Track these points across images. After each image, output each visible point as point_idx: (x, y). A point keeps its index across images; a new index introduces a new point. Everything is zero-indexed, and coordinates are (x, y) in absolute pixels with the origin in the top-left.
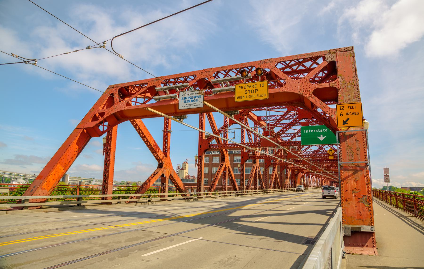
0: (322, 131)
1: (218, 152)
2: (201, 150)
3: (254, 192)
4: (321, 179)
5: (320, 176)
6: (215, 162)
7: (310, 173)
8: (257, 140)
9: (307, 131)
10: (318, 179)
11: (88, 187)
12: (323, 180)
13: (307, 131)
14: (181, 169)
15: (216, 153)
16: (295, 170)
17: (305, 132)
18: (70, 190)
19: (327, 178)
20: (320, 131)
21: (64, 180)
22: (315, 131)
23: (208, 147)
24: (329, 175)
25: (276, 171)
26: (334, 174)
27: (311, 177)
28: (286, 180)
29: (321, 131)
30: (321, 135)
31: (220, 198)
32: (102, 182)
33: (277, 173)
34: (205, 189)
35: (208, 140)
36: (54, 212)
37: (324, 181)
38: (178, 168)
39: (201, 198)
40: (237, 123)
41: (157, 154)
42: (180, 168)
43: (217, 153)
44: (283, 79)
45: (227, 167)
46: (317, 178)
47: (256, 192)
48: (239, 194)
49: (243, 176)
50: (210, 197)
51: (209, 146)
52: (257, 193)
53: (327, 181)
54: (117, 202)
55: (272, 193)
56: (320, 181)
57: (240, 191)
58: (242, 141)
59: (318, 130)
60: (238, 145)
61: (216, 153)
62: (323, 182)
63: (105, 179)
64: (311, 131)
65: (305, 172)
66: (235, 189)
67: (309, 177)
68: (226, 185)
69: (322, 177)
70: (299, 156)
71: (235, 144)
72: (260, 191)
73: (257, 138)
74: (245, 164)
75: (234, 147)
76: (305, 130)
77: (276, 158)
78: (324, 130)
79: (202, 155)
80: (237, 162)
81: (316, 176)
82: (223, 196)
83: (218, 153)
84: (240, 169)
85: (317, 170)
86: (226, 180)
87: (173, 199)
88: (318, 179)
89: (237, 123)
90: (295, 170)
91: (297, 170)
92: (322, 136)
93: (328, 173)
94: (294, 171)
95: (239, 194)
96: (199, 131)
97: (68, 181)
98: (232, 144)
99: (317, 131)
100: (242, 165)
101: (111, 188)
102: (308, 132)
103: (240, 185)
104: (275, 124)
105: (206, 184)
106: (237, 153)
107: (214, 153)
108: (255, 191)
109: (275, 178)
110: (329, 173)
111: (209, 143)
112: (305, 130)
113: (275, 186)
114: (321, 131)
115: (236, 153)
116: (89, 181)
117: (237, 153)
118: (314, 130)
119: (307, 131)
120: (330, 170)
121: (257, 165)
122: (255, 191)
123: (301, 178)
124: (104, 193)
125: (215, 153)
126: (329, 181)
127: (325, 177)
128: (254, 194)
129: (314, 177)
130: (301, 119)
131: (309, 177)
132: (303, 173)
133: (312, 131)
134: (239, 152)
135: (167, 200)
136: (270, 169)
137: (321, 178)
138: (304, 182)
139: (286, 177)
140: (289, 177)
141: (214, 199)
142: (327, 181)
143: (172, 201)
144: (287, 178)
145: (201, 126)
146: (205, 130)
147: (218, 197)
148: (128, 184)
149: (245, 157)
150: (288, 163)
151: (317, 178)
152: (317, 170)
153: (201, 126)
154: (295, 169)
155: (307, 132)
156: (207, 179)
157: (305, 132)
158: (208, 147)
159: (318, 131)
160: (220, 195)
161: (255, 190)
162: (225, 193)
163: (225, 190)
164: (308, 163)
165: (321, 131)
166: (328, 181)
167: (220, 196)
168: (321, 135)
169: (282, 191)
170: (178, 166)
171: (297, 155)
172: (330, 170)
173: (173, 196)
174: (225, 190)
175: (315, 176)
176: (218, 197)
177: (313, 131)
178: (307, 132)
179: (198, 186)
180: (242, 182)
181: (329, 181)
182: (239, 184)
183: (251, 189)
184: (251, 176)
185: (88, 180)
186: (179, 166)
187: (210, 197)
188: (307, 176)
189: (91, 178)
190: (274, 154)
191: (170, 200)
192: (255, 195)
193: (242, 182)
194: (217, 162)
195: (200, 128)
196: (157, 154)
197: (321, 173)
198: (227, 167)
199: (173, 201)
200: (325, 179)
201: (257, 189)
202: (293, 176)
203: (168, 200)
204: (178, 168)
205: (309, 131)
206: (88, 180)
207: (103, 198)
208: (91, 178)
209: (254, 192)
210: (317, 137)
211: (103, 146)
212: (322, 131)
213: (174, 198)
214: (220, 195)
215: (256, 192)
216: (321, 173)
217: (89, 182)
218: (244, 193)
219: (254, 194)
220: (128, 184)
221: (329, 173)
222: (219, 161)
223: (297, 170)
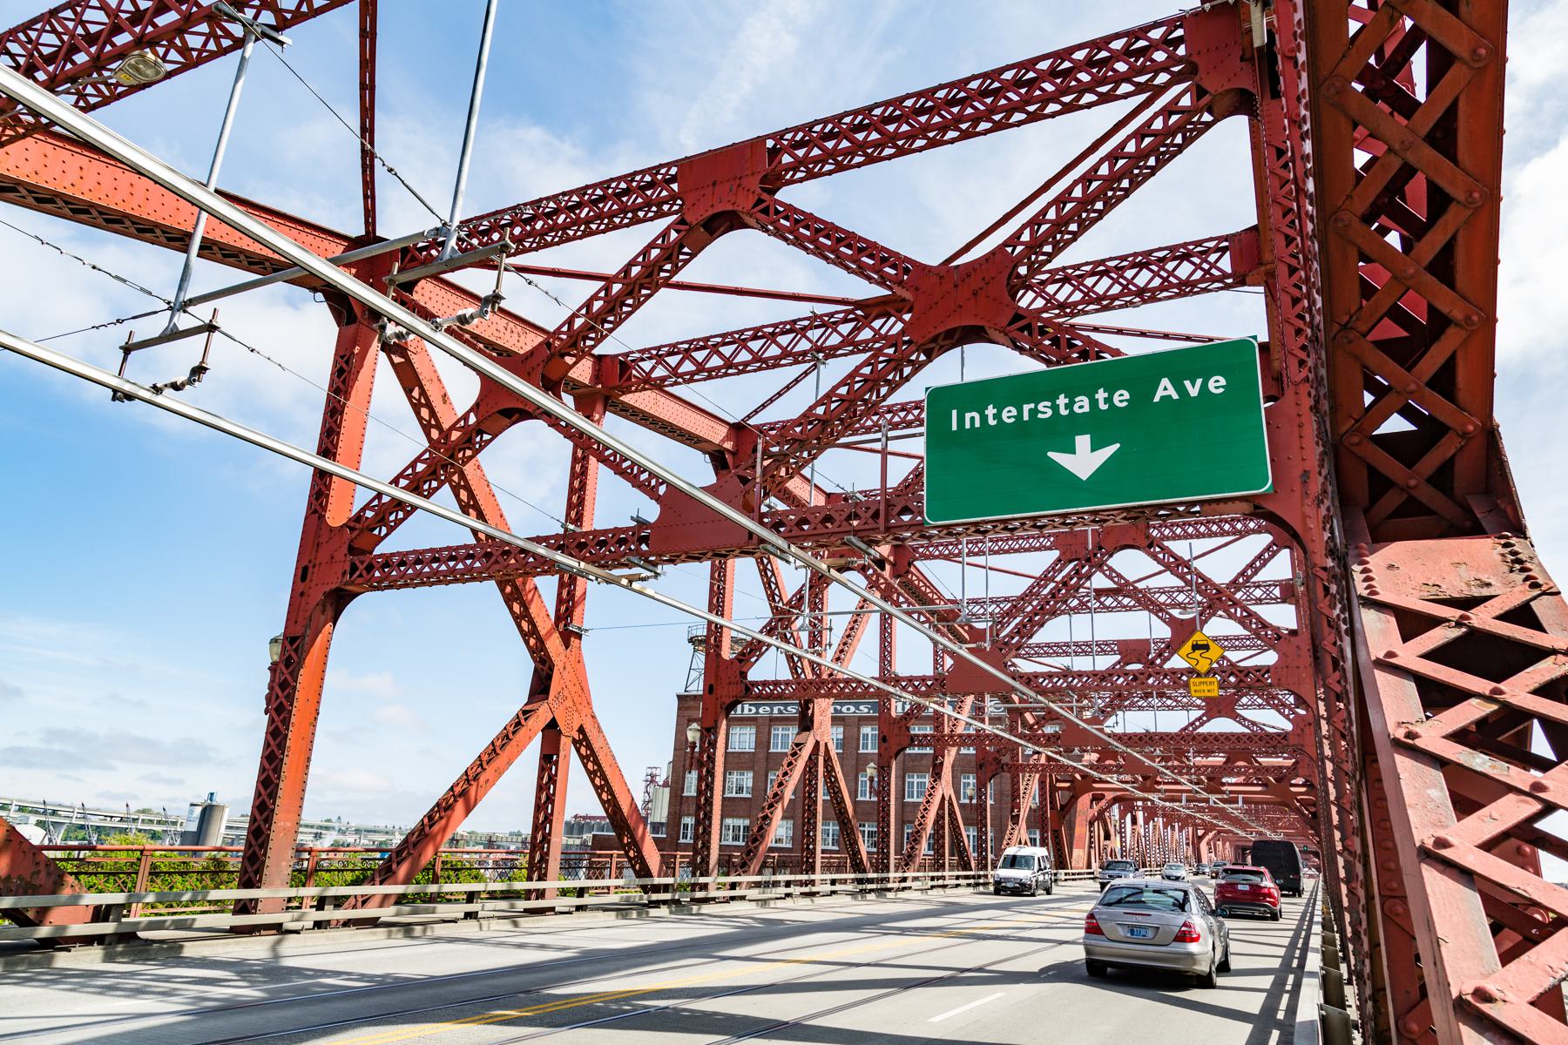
0: (1086, 409)
1: (750, 705)
2: (302, 594)
3: (933, 879)
4: (1195, 832)
5: (1185, 821)
6: (737, 750)
7: (1140, 803)
8: (943, 666)
9: (972, 419)
10: (1180, 830)
11: (200, 856)
12: (1200, 838)
13: (972, 419)
14: (661, 783)
15: (743, 710)
16: (1059, 785)
17: (954, 428)
18: (99, 870)
19: (1219, 832)
20: (1072, 411)
21: (204, 826)
22: (1034, 412)
23: (344, 574)
24: (1223, 814)
25: (943, 781)
26: (1247, 812)
27: (1146, 822)
28: (1010, 828)
29: (1082, 404)
30: (1078, 439)
31: (789, 903)
33: (950, 792)
34: (681, 863)
35: (740, 661)
37: (1208, 844)
38: (652, 781)
39: (706, 901)
42: (657, 779)
43: (746, 711)
45: (947, 798)
46: (1173, 828)
47: (941, 882)
48: (870, 886)
49: (888, 815)
50: (743, 898)
51: (348, 569)
52: (944, 886)
53: (1220, 843)
54: (462, 915)
55: (918, 895)
56: (1188, 844)
57: (875, 875)
58: (882, 669)
59: (1053, 398)
60: (870, 686)
61: (743, 710)
62: (1203, 846)
64: (1005, 415)
65: (1109, 796)
66: (858, 866)
67: (1134, 821)
68: (814, 849)
69: (1196, 826)
70: (1014, 679)
71: (860, 682)
72: (958, 878)
73: (942, 657)
74: (894, 766)
75: (851, 690)
76: (954, 412)
77: (1021, 745)
78: (1101, 395)
79: (716, 722)
81: (1170, 818)
82: (802, 894)
83: (750, 710)
84: (974, 801)
85: (1160, 787)
86: (815, 828)
87: (579, 908)
88: (1180, 831)
90: (1059, 785)
91: (1067, 785)
92: (1083, 442)
93: (1215, 803)
94: (1054, 789)
95: (870, 886)
96: (710, 623)
97: (223, 830)
98: (847, 682)
99: (1050, 412)
100: (883, 768)
101: (279, 861)
102: (977, 424)
103: (875, 850)
104: (1036, 614)
105: (830, 847)
108: (939, 878)
109: (940, 817)
110: (1221, 805)
111: (744, 675)
112: (954, 412)
113: (986, 858)
114: (1082, 404)
116: (315, 831)
118: (1026, 408)
119: (968, 416)
120: (1224, 788)
121: (817, 743)
122: (939, 878)
123: (1091, 824)
124: (247, 883)
126: (1228, 843)
127: (1208, 828)
128: (932, 887)
129: (1160, 821)
130: (1219, 712)
131: (1134, 821)
132: (1103, 803)
133: (1008, 415)
134: (779, 710)
135: (552, 909)
137: (1190, 829)
138: (1107, 842)
139: (1012, 817)
140: (1024, 814)
141: (389, 937)
142: (1220, 843)
143: (576, 914)
144: (1015, 819)
145: (717, 601)
146: (730, 619)
147: (781, 898)
148: (457, 841)
149: (895, 736)
150: (988, 736)
151: (1173, 828)
152: (1160, 787)
153: (717, 601)
154: (1057, 781)
155: (968, 426)
156: (747, 822)
157: (954, 428)
158: (344, 574)
159: (1055, 408)
160: (788, 890)
161: (935, 874)
162: (812, 882)
163: (811, 869)
164: (1085, 729)
165: (1076, 409)
166: (1224, 844)
167: (788, 895)
168: (1078, 439)
169: (981, 881)
170: (649, 771)
171: (1096, 729)
172: (1224, 788)
173: (581, 892)
174: (811, 869)
175: (1163, 817)
176: (781, 898)
177: (1014, 412)
178: (968, 426)
179: (696, 852)
180: (881, 840)
181: (1228, 843)
182: (833, 845)
183: (922, 867)
184: (776, 795)
185: (312, 827)
186: (654, 771)
187: (743, 898)
188: (1122, 816)
189: (326, 821)
190: (1003, 727)
191: (566, 909)
192: (934, 892)
193: (881, 840)
194: (747, 750)
195: (710, 611)
197: (1184, 803)
198: (947, 798)
199: (581, 914)
200: (1211, 835)
201: (814, 872)
202: (1046, 812)
203: (557, 909)
204: (652, 781)
205: (984, 418)
206: (312, 827)
207: (244, 907)
208: (329, 821)
209: (933, 879)
211: (269, 672)
212: (1086, 409)
213: (587, 900)
214: (788, 890)
215: (941, 882)
216: (1184, 803)
217: (316, 834)
218: (889, 885)
219: (932, 887)
220: (457, 841)
221: (1221, 805)
222: (753, 745)
223: (1067, 785)
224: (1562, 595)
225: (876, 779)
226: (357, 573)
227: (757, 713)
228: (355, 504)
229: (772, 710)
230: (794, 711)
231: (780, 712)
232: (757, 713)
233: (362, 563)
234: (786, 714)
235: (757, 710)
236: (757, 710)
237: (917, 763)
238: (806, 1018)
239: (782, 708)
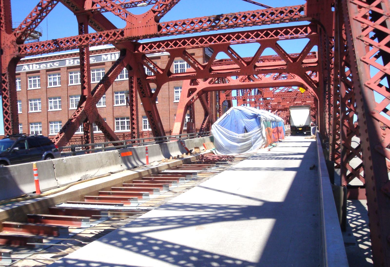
15: (33, 68)
32: (18, 99)
36: (48, 126)
40: (38, 69)
41: (25, 39)
44: (96, 243)
61: (33, 68)
63: (80, 29)
76: (229, 51)
80: (121, 79)
83: (36, 67)
89: (38, 69)
106: (74, 64)
107: (29, 68)
112: (229, 51)
115: (72, 63)
117: (74, 62)
125: (31, 68)
134: (50, 65)
136: (70, 76)
196: (25, 39)
210: (316, 33)
224: (385, 138)
225: (214, 119)
226: (22, 51)
227: (40, 68)
228: (236, 11)
229: (47, 66)
230: (58, 65)
231: (51, 66)
232: (40, 68)
233: (104, 34)
234: (54, 67)
235: (40, 66)
236: (40, 66)
237: (119, 86)
238: (340, 223)
239: (51, 64)
